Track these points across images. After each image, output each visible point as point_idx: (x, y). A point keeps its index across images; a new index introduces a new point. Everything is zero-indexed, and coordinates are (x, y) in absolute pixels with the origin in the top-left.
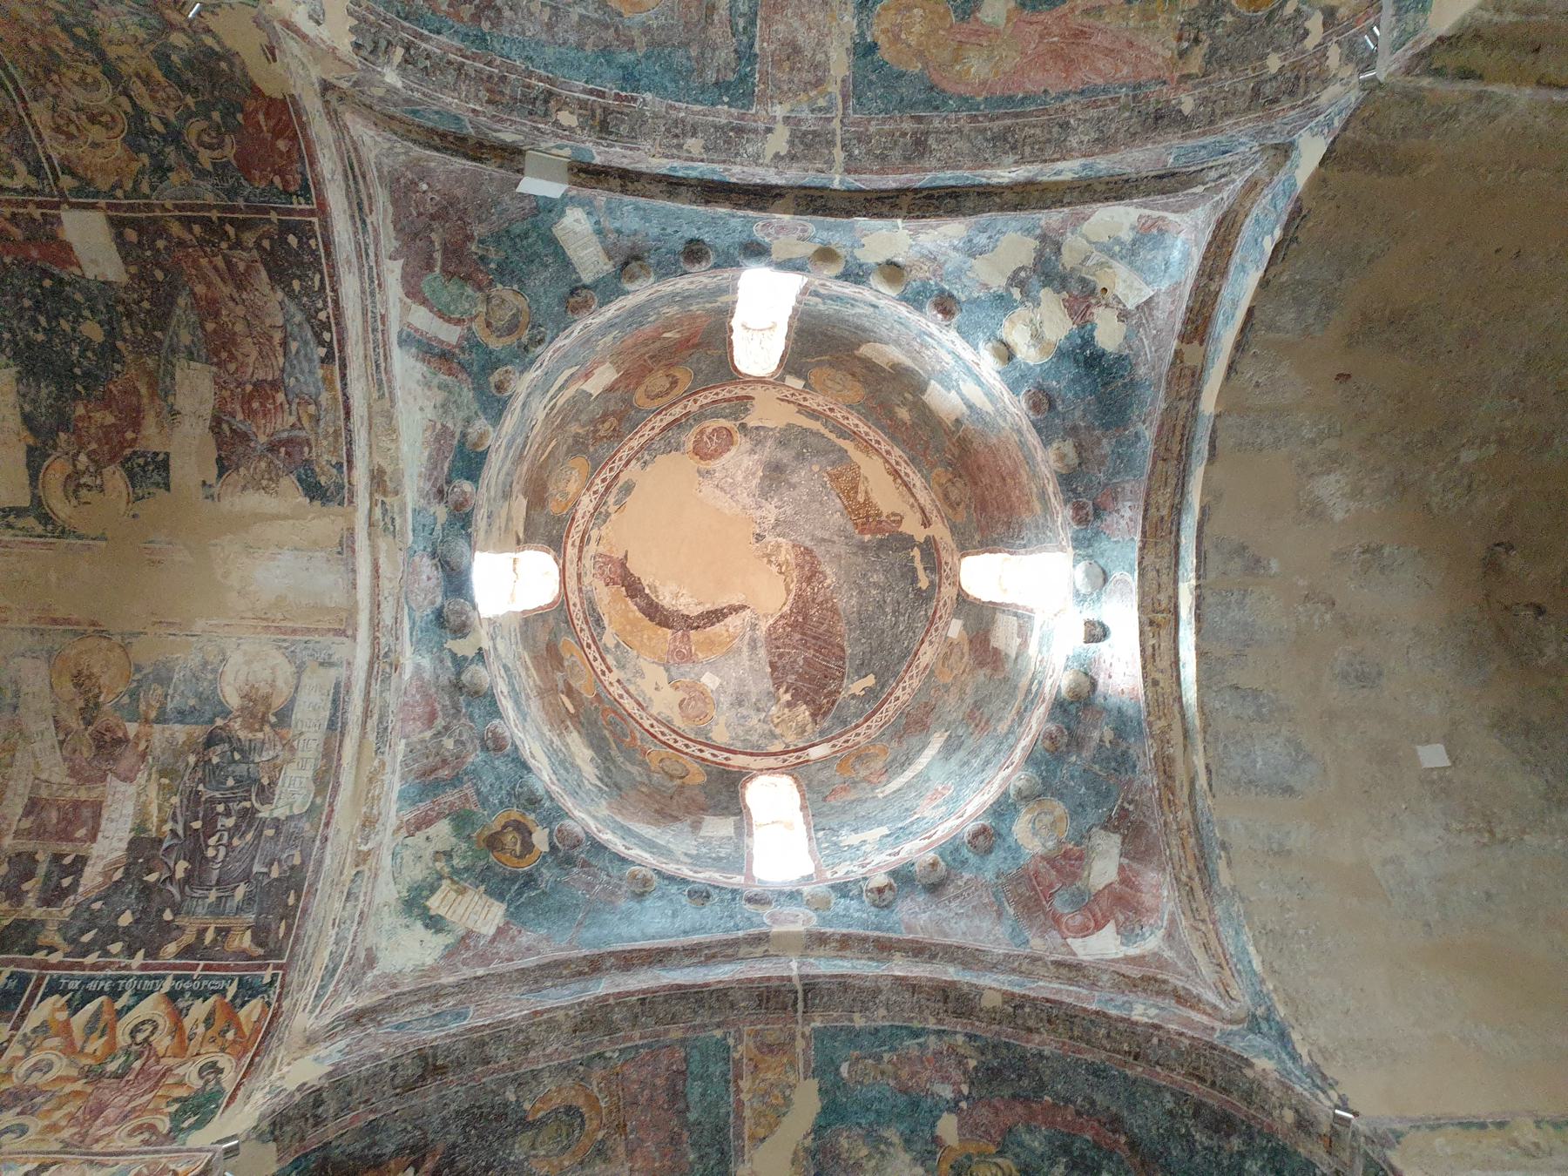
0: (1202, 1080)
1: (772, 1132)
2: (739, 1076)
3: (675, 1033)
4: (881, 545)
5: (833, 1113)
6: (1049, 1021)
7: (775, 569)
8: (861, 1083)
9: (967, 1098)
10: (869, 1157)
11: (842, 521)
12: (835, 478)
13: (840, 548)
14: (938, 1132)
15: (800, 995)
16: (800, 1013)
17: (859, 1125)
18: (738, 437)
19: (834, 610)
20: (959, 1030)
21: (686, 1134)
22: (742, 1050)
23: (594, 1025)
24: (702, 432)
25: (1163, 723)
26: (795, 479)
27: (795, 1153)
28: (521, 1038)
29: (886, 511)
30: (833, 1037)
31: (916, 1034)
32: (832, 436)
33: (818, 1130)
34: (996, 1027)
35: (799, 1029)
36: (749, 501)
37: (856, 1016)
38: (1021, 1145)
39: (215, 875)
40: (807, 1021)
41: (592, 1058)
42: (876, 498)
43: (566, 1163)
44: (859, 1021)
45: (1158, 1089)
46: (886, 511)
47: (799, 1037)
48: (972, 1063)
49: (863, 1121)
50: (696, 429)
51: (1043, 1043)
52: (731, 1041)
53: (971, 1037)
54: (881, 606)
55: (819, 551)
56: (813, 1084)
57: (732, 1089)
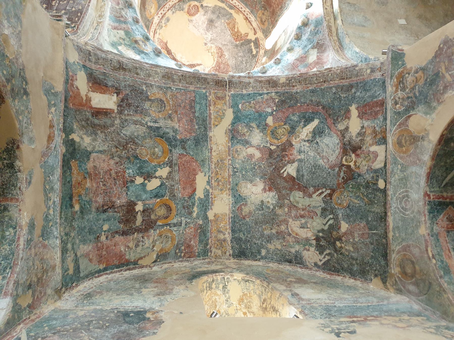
0: (343, 79)
1: (220, 124)
2: (210, 105)
3: (192, 88)
4: (242, 44)
5: (237, 119)
6: (299, 82)
7: (210, 54)
8: (245, 110)
9: (275, 111)
10: (247, 132)
11: (230, 38)
12: (228, 24)
13: (230, 47)
14: (267, 122)
15: (228, 83)
16: (227, 89)
17: (244, 122)
18: (200, 9)
19: (228, 65)
20: (273, 91)
21: (195, 120)
22: (211, 98)
23: (169, 78)
24: (190, 6)
25: (328, 18)
26: (216, 25)
27: (226, 131)
28: (147, 72)
29: (243, 33)
30: (237, 97)
31: (261, 95)
32: (228, 9)
33: (233, 124)
34: (284, 88)
35: (227, 93)
36: (203, 32)
37: (244, 90)
38: (291, 120)
39: (55, 8)
40: (230, 91)
41: (168, 87)
42: (240, 29)
43: (160, 116)
44: (244, 92)
45: (331, 88)
46: (243, 33)
47: (227, 95)
48: (277, 100)
49: (245, 121)
50: (188, 4)
51: (298, 89)
52: (208, 94)
53: (276, 93)
54: (242, 62)
55: (223, 48)
56: (231, 110)
57: (208, 109)
